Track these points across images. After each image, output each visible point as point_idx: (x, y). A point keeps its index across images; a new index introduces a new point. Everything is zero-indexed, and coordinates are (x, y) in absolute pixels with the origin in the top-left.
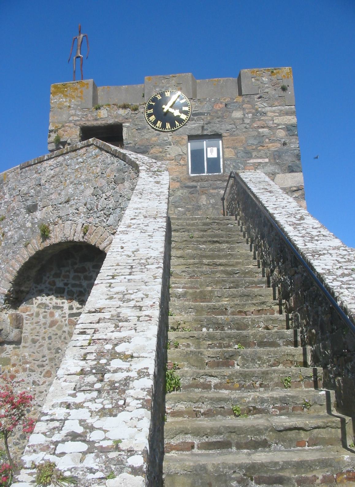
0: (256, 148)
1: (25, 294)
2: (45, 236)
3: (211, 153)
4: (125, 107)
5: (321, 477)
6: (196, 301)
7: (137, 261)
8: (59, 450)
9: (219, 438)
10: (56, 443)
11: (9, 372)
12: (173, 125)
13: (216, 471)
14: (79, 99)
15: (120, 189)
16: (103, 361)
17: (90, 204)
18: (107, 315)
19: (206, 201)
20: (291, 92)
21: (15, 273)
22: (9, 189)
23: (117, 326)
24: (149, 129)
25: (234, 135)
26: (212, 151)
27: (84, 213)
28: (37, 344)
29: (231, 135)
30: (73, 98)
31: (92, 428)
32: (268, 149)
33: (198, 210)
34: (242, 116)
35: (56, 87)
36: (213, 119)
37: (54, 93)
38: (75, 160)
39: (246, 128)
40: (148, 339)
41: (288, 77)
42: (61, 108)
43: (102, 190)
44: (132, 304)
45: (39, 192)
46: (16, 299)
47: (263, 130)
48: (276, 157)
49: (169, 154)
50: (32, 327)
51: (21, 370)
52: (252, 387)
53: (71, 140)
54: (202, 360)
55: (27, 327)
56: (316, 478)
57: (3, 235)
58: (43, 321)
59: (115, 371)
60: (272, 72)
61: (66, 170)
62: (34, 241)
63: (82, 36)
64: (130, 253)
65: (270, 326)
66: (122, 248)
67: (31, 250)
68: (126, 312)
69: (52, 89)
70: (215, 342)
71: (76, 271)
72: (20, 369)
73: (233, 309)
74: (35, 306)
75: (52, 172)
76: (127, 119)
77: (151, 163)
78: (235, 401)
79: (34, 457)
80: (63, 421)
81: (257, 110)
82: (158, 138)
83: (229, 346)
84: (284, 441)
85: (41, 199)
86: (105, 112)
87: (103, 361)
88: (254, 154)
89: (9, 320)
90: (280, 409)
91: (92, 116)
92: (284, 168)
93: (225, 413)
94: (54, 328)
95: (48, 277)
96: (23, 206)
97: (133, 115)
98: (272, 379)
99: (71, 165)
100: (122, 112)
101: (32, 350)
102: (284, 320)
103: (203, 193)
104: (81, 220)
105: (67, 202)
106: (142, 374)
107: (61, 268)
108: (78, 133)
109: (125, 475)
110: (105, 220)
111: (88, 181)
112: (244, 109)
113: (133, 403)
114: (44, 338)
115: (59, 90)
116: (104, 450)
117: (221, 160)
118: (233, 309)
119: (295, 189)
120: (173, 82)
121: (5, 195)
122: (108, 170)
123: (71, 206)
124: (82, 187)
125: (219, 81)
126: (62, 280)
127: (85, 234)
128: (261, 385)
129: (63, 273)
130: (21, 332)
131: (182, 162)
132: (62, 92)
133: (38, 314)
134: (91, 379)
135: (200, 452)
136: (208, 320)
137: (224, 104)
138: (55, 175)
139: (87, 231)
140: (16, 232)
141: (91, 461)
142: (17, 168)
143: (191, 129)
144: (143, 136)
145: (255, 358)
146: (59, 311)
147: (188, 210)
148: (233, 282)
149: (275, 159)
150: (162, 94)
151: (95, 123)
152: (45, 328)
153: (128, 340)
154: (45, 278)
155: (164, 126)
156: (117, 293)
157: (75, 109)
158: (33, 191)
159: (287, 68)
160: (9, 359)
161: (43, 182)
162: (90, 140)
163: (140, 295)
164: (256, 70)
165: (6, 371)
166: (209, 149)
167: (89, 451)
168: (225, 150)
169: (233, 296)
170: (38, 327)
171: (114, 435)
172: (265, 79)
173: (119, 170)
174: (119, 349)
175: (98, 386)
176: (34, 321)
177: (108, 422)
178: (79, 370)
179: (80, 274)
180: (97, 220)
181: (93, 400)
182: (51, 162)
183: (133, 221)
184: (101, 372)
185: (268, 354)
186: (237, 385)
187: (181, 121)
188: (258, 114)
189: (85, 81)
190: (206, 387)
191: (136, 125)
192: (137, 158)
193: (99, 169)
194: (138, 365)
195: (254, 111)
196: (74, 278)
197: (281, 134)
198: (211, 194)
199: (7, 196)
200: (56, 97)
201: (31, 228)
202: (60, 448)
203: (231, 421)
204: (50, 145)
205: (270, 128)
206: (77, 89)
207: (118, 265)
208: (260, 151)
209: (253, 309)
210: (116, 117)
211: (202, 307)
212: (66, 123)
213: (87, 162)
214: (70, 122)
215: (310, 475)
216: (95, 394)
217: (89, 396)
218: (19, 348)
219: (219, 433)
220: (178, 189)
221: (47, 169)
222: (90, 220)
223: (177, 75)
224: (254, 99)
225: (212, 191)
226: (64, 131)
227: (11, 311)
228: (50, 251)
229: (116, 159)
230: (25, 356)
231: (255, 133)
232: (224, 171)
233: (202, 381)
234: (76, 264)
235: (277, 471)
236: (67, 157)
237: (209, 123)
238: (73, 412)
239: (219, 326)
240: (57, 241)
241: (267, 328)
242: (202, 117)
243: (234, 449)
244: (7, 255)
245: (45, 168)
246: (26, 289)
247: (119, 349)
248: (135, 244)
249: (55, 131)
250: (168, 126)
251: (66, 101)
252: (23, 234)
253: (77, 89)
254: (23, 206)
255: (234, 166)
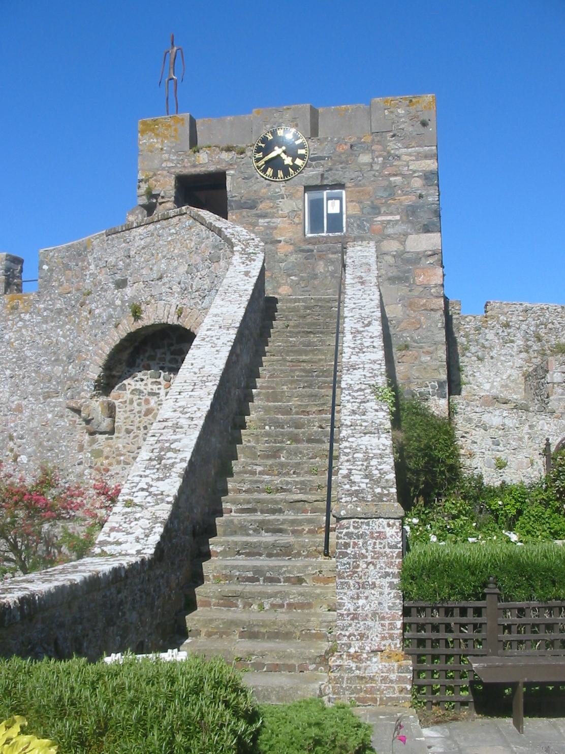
0: (386, 202)
1: (116, 379)
2: (136, 313)
3: (332, 207)
4: (229, 149)
5: (307, 530)
6: (268, 401)
7: (200, 379)
8: (135, 495)
9: (249, 506)
10: (134, 492)
11: (102, 465)
12: (286, 174)
13: (240, 523)
14: (173, 140)
15: (215, 268)
16: (162, 453)
17: (185, 283)
18: (170, 424)
19: (324, 268)
20: (431, 128)
21: (105, 357)
22: (94, 258)
23: (175, 431)
24: (257, 178)
25: (360, 186)
26: (333, 205)
27: (178, 293)
28: (132, 435)
29: (356, 185)
30: (166, 137)
31: (152, 486)
32: (401, 203)
33: (315, 279)
34: (371, 161)
35: (144, 123)
36: (334, 164)
37: (143, 132)
38: (167, 230)
39: (374, 176)
40: (192, 440)
41: (430, 108)
42: (151, 152)
43: (197, 269)
44: (188, 415)
45: (129, 265)
46: (106, 384)
47: (395, 178)
48: (410, 213)
49: (282, 210)
50: (126, 416)
51: (115, 463)
52: (287, 474)
53: (165, 192)
54: (255, 453)
55: (120, 415)
56: (304, 530)
57: (90, 313)
58: (137, 408)
59: (168, 459)
60: (411, 101)
61: (158, 241)
62: (125, 321)
63: (175, 48)
64: (197, 371)
65: (324, 426)
66: (192, 364)
67: (122, 331)
68: (183, 422)
69: (140, 126)
70: (271, 439)
71: (172, 354)
72: (114, 461)
73: (297, 409)
74: (128, 392)
75: (142, 242)
76: (231, 164)
77: (249, 239)
78: (268, 483)
79: (123, 497)
80: (138, 483)
81: (389, 152)
82: (269, 191)
83: (282, 442)
84: (294, 509)
85: (131, 274)
86: (206, 156)
87: (162, 453)
88: (383, 210)
89: (100, 409)
90: (300, 489)
91: (190, 162)
92: (418, 227)
93: (259, 491)
94: (150, 417)
95: (142, 360)
96: (111, 280)
97: (239, 160)
98: (302, 469)
99: (163, 236)
100: (225, 156)
101: (126, 441)
102: (328, 420)
103: (321, 258)
104: (174, 301)
105: (160, 278)
106: (182, 460)
107: (156, 350)
108: (173, 183)
109: (163, 504)
110: (200, 302)
111: (182, 256)
112: (373, 151)
113: (174, 475)
114: (138, 428)
115: (148, 128)
116: (155, 495)
117: (344, 217)
118: (297, 409)
119: (430, 253)
120: (288, 116)
121: (89, 265)
122: (203, 245)
123: (164, 284)
124: (176, 264)
125: (347, 110)
126: (158, 364)
127: (179, 317)
128: (294, 473)
129: (159, 356)
130: (114, 422)
131: (297, 220)
132: (153, 130)
133: (132, 402)
134: (155, 463)
135: (236, 515)
136: (270, 419)
137: (349, 145)
138: (146, 246)
139: (181, 313)
140: (104, 310)
141: (149, 499)
142: (103, 234)
143: (309, 178)
144: (250, 187)
145: (296, 452)
146: (155, 397)
147: (302, 279)
148: (307, 382)
149: (408, 216)
150: (274, 133)
151: (194, 171)
152: (140, 417)
153: (178, 440)
154: (138, 361)
155: (275, 175)
156: (180, 407)
157: (169, 153)
158: (121, 263)
159: (429, 95)
160: (102, 451)
161: (132, 253)
162: (183, 208)
163: (195, 408)
164: (390, 98)
165: (99, 464)
166: (330, 202)
167: (149, 495)
168: (349, 204)
169: (301, 396)
170: (132, 416)
171: (161, 489)
172: (401, 111)
173: (215, 247)
174: (172, 446)
175: (158, 466)
176: (128, 409)
177: (160, 483)
178: (148, 458)
179: (176, 357)
180: (192, 301)
181: (154, 473)
182: (141, 230)
183: (209, 333)
184: (160, 459)
185: (307, 449)
186: (276, 472)
187: (295, 167)
188: (389, 157)
189: (180, 116)
190: (253, 473)
191: (242, 173)
192: (233, 234)
193: (193, 244)
194: (181, 456)
195: (385, 154)
196: (170, 362)
197: (417, 183)
198: (330, 259)
199: (92, 267)
200: (145, 136)
201: (121, 307)
202: (136, 494)
203: (264, 496)
204: (140, 198)
205: (404, 176)
206: (170, 126)
207: (185, 382)
208: (390, 205)
209: (315, 409)
210: (218, 163)
211: (270, 407)
212: (158, 170)
213: (180, 234)
214: (163, 169)
215: (300, 528)
216: (155, 470)
217: (152, 471)
218: (112, 438)
219: (249, 502)
220: (291, 253)
221: (137, 238)
222: (184, 301)
223: (293, 106)
224: (386, 137)
225: (330, 256)
226: (156, 181)
227: (103, 399)
228: (143, 333)
229: (211, 233)
230: (118, 448)
231: (386, 183)
232: (347, 230)
233: (249, 468)
234: (172, 345)
235: (280, 524)
236: (158, 226)
237: (330, 169)
238: (143, 479)
239: (279, 424)
240: (151, 322)
241: (321, 427)
242: (322, 162)
243: (259, 513)
244: (96, 336)
245: (134, 237)
246: (118, 374)
247: (172, 446)
248: (203, 360)
249: (146, 181)
250: (280, 174)
251: (158, 142)
252: (113, 312)
253: (170, 126)
254: (111, 280)
255: (358, 225)
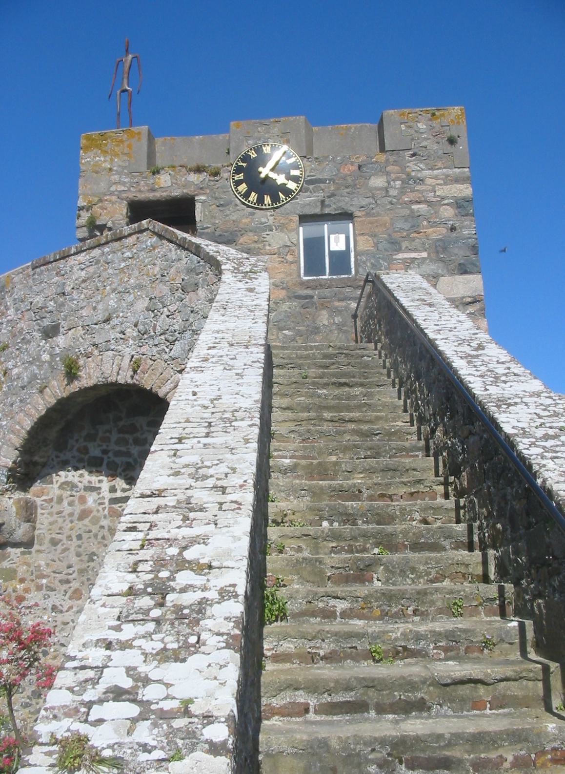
0: (408, 235)
1: (39, 467)
2: (71, 374)
3: (336, 243)
4: (199, 170)
5: (510, 758)
6: (311, 478)
7: (218, 415)
8: (94, 715)
9: (348, 697)
10: (89, 705)
11: (14, 591)
12: (275, 199)
13: (344, 749)
14: (126, 158)
15: (190, 300)
16: (164, 574)
17: (144, 324)
18: (171, 501)
19: (328, 319)
20: (462, 146)
21: (24, 434)
22: (15, 300)
23: (186, 518)
24: (236, 205)
25: (373, 215)
26: (337, 241)
27: (134, 339)
28: (60, 547)
29: (368, 215)
30: (117, 155)
31: (146, 681)
32: (427, 237)
33: (316, 334)
34: (386, 184)
35: (88, 138)
36: (338, 189)
37: (87, 149)
38: (119, 254)
39: (391, 203)
40: (236, 539)
41: (458, 123)
42: (97, 172)
43: (162, 303)
44: (210, 482)
45: (62, 305)
46: (25, 475)
47: (418, 206)
48: (439, 249)
49: (269, 245)
50: (51, 519)
51: (33, 588)
52: (401, 616)
53: (113, 223)
54: (322, 572)
55: (43, 519)
56: (502, 759)
57: (5, 373)
58: (68, 510)
59: (183, 590)
60: (433, 114)
61: (105, 270)
62: (54, 383)
63: (130, 56)
64: (207, 403)
65: (430, 519)
66: (194, 394)
67: (50, 397)
68: (200, 496)
69: (83, 142)
70: (343, 544)
71: (120, 431)
72: (32, 586)
73: (370, 492)
74: (56, 486)
75: (83, 273)
76: (201, 189)
77: (241, 259)
78: (375, 637)
79: (53, 726)
80: (100, 669)
81: (408, 175)
82: (252, 219)
83: (364, 550)
84: (451, 701)
85: (66, 316)
86: (168, 178)
87: (164, 574)
88: (404, 245)
89: (14, 509)
90: (446, 650)
91: (147, 185)
92: (452, 266)
93: (357, 656)
94: (86, 521)
95: (77, 441)
96: (37, 327)
97: (212, 183)
98: (432, 603)
99: (112, 262)
100: (193, 178)
101: (51, 556)
102: (452, 509)
103: (324, 306)
104: (128, 350)
105: (107, 320)
106: (226, 594)
107: (98, 427)
108: (125, 211)
109: (199, 755)
110: (167, 350)
111: (140, 287)
112: (388, 174)
113: (212, 641)
114: (69, 538)
115: (93, 144)
116: (165, 716)
117: (352, 255)
118: (370, 492)
119: (469, 300)
120: (276, 130)
121: (7, 309)
122: (173, 270)
123: (113, 328)
124: (131, 298)
125: (349, 129)
126: (99, 446)
127: (135, 372)
128: (415, 612)
129: (101, 434)
130: (34, 528)
131: (290, 258)
132: (99, 147)
133: (60, 500)
134: (145, 602)
135: (318, 718)
136: (332, 508)
137: (356, 165)
138: (88, 278)
139: (139, 367)
140: (26, 368)
141: (144, 733)
142: (28, 267)
143: (304, 205)
144: (227, 216)
145: (405, 570)
146: (95, 494)
147: (299, 334)
148: (370, 449)
149: (437, 252)
150: (258, 150)
151: (151, 196)
152: (72, 522)
153: (203, 540)
154: (71, 442)
155: (260, 200)
156: (187, 466)
157: (119, 173)
158: (52, 303)
159: (456, 108)
160: (15, 571)
161: (68, 289)
162: (144, 222)
163: (223, 468)
164: (407, 111)
165: (10, 590)
166: (332, 237)
167: (142, 717)
168: (358, 238)
169: (370, 471)
170: (60, 520)
171: (182, 691)
172: (422, 126)
173: (190, 271)
174: (189, 555)
175: (156, 613)
176: (55, 510)
177: (171, 671)
178: (125, 587)
179: (127, 436)
180: (155, 349)
181: (148, 636)
182: (81, 257)
183: (212, 352)
184: (160, 591)
185: (426, 563)
186: (378, 612)
187: (287, 192)
188: (410, 181)
189: (135, 129)
190: (328, 615)
191: (216, 198)
192: (217, 252)
193: (157, 269)
194: (219, 580)
195: (404, 176)
196: (117, 443)
197: (448, 212)
198: (336, 308)
199: (11, 312)
200: (89, 154)
201: (49, 363)
202: (96, 713)
203: (367, 669)
204: (80, 230)
205: (429, 203)
206: (122, 141)
207: (188, 421)
208: (413, 239)
209: (402, 490)
210: (184, 186)
211: (321, 488)
212: (105, 195)
213: (138, 257)
214: (112, 194)
215: (493, 755)
216: (151, 626)
217: (141, 629)
218: (30, 553)
219: (348, 688)
220: (283, 300)
221: (75, 269)
222: (143, 350)
223: (282, 119)
224: (404, 157)
225: (337, 304)
226: (103, 208)
227: (18, 495)
228: (80, 399)
229: (184, 253)
230: (39, 566)
231: (406, 212)
232: (357, 271)
233: (321, 605)
234: (120, 419)
235: (441, 748)
236: (106, 249)
237: (333, 195)
238: (116, 655)
239: (349, 518)
240: (91, 383)
241: (425, 521)
242: (322, 186)
243: (373, 714)
244: (12, 405)
245: (72, 267)
246: (42, 460)
247: (189, 555)
248: (215, 388)
249: (88, 208)
250: (267, 200)
251: (105, 161)
252: (37, 371)
253: (122, 141)
254: (37, 327)
255: (372, 264)
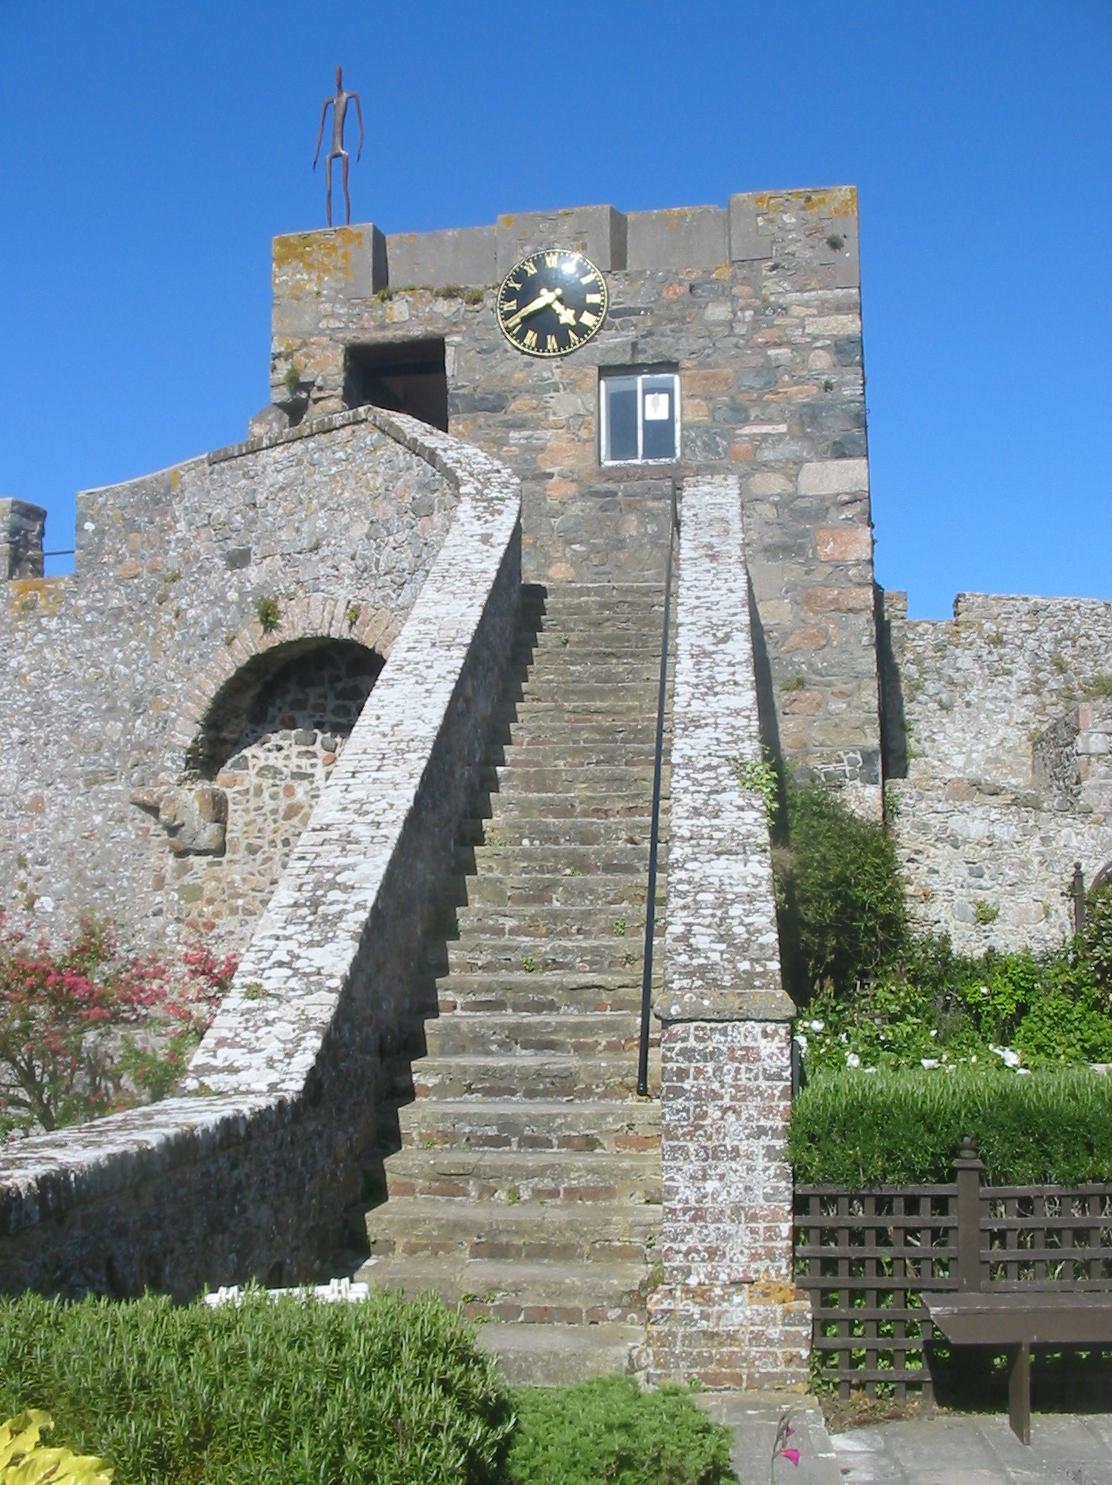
0: (760, 398)
1: (229, 747)
2: (269, 617)
3: (654, 408)
4: (450, 294)
5: (604, 1043)
6: (528, 789)
7: (393, 746)
8: (265, 975)
9: (490, 997)
10: (263, 970)
11: (200, 916)
12: (563, 342)
13: (472, 1031)
14: (340, 275)
15: (423, 528)
16: (320, 893)
17: (363, 557)
18: (334, 834)
19: (637, 528)
20: (849, 253)
21: (207, 703)
22: (186, 508)
23: (344, 849)
24: (506, 351)
25: (709, 366)
26: (655, 404)
27: (351, 577)
28: (259, 856)
29: (701, 365)
30: (326, 270)
31: (298, 957)
32: (789, 399)
33: (619, 549)
34: (730, 316)
35: (284, 243)
36: (658, 324)
37: (282, 260)
38: (329, 452)
39: (737, 346)
40: (378, 867)
41: (846, 213)
42: (298, 299)
43: (387, 529)
44: (369, 818)
45: (253, 521)
46: (209, 757)
47: (777, 351)
48: (806, 419)
49: (554, 414)
50: (248, 818)
51: (226, 912)
52: (566, 933)
53: (324, 379)
54: (502, 893)
55: (236, 818)
56: (597, 1043)
57: (177, 616)
58: (270, 804)
59: (331, 904)
60: (809, 199)
61: (310, 475)
62: (246, 633)
63: (345, 95)
64: (387, 730)
65: (637, 838)
66: (378, 718)
67: (240, 652)
68: (361, 831)
69: (276, 249)
70: (533, 864)
71: (338, 696)
72: (224, 908)
73: (584, 806)
74: (253, 772)
75: (280, 477)
76: (455, 324)
77: (490, 472)
78: (527, 950)
79: (243, 980)
80: (271, 952)
81: (765, 300)
82: (529, 375)
83: (555, 870)
84: (578, 1003)
85: (258, 539)
86: (405, 307)
87: (320, 893)
88: (753, 413)
89: (197, 805)
90: (591, 963)
91: (373, 318)
92: (823, 447)
93: (511, 967)
94: (295, 821)
95: (280, 709)
96: (219, 552)
97: (470, 315)
98: (595, 923)
99: (320, 464)
100: (443, 307)
101: (247, 868)
102: (646, 827)
103: (631, 508)
104: (343, 593)
105: (316, 548)
106: (358, 906)
107: (308, 690)
108: (341, 360)
109: (321, 992)
110: (394, 596)
111: (358, 504)
112: (734, 298)
113: (342, 935)
114: (273, 843)
115: (292, 253)
116: (306, 975)
117: (678, 426)
118: (584, 806)
119: (846, 498)
120: (566, 228)
121: (176, 522)
122: (400, 483)
123: (322, 560)
124: (346, 519)
125: (682, 217)
126: (311, 716)
127: (352, 623)
128: (579, 931)
129: (312, 700)
130: (225, 831)
131: (584, 434)
132: (300, 257)
133: (259, 791)
134: (304, 911)
135: (464, 1014)
136: (532, 825)
137: (687, 285)
138: (288, 485)
139: (357, 617)
140: (206, 611)
141: (293, 983)
142: (202, 461)
143: (608, 350)
144: (492, 367)
145: (583, 891)
146: (306, 782)
147: (595, 549)
148: (603, 752)
149: (802, 425)
150: (539, 262)
151: (381, 336)
152: (275, 821)
153: (351, 867)
154: (272, 711)
155: (541, 344)
156: (354, 802)
157: (333, 301)
158: (238, 517)
159: (844, 188)
160: (201, 889)
161: (260, 498)
162: (361, 409)
163: (383, 804)
164: (767, 193)
165: (195, 914)
166: (649, 397)
167: (293, 976)
168: (686, 402)
169: (592, 781)
170: (260, 819)
171: (317, 963)
172: (788, 219)
173: (423, 486)
174: (339, 879)
175: (310, 918)
176: (251, 805)
177: (314, 952)
178: (291, 902)
179: (347, 703)
180: (379, 594)
181: (303, 932)
182: (277, 453)
183: (411, 656)
184: (315, 903)
185: (605, 885)
186: (544, 930)
187: (581, 330)
188: (766, 309)
189: (353, 228)
190: (498, 931)
191: (476, 340)
192: (458, 462)
193: (380, 480)
194: (356, 897)
195: (758, 303)
196: (335, 712)
197: (821, 360)
198: (650, 510)
199: (181, 526)
200: (286, 268)
201: (238, 604)
202: (267, 974)
203: (520, 976)
204: (276, 390)
205: (794, 346)
206: (334, 248)
207: (365, 752)
208: (767, 404)
209: (620, 805)
210: (430, 321)
211: (530, 801)
212: (311, 335)
213: (354, 460)
214: (322, 333)
215: (590, 1040)
216: (306, 927)
217: (299, 928)
218: (220, 864)
219: (489, 989)
220: (573, 498)
221: (269, 469)
222: (363, 593)
223: (577, 209)
224: (759, 271)
225: (650, 504)
226: (308, 356)
227: (203, 785)
228: (281, 655)
229: (416, 458)
230: (233, 882)
231: (759, 361)
232: (683, 454)
233: (491, 922)
234: (338, 679)
235: (551, 1033)
236: (312, 445)
237: (650, 334)
238: (282, 943)
239: (549, 836)
240: (297, 634)
241: (631, 841)
242: (634, 319)
243: (510, 1011)
244: (188, 661)
245: (264, 467)
246: (232, 736)
247: (339, 879)
248: (399, 709)
249: (288, 356)
250: (552, 342)
251: (310, 280)
252: (221, 615)
253: (334, 248)
254: (219, 552)
255: (704, 442)
